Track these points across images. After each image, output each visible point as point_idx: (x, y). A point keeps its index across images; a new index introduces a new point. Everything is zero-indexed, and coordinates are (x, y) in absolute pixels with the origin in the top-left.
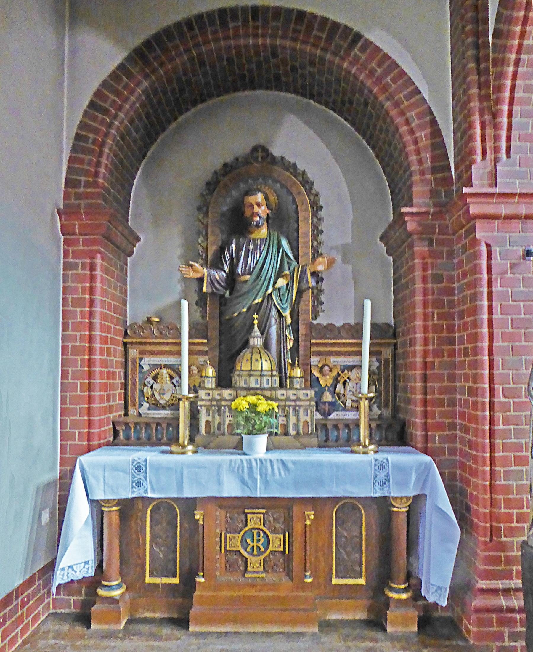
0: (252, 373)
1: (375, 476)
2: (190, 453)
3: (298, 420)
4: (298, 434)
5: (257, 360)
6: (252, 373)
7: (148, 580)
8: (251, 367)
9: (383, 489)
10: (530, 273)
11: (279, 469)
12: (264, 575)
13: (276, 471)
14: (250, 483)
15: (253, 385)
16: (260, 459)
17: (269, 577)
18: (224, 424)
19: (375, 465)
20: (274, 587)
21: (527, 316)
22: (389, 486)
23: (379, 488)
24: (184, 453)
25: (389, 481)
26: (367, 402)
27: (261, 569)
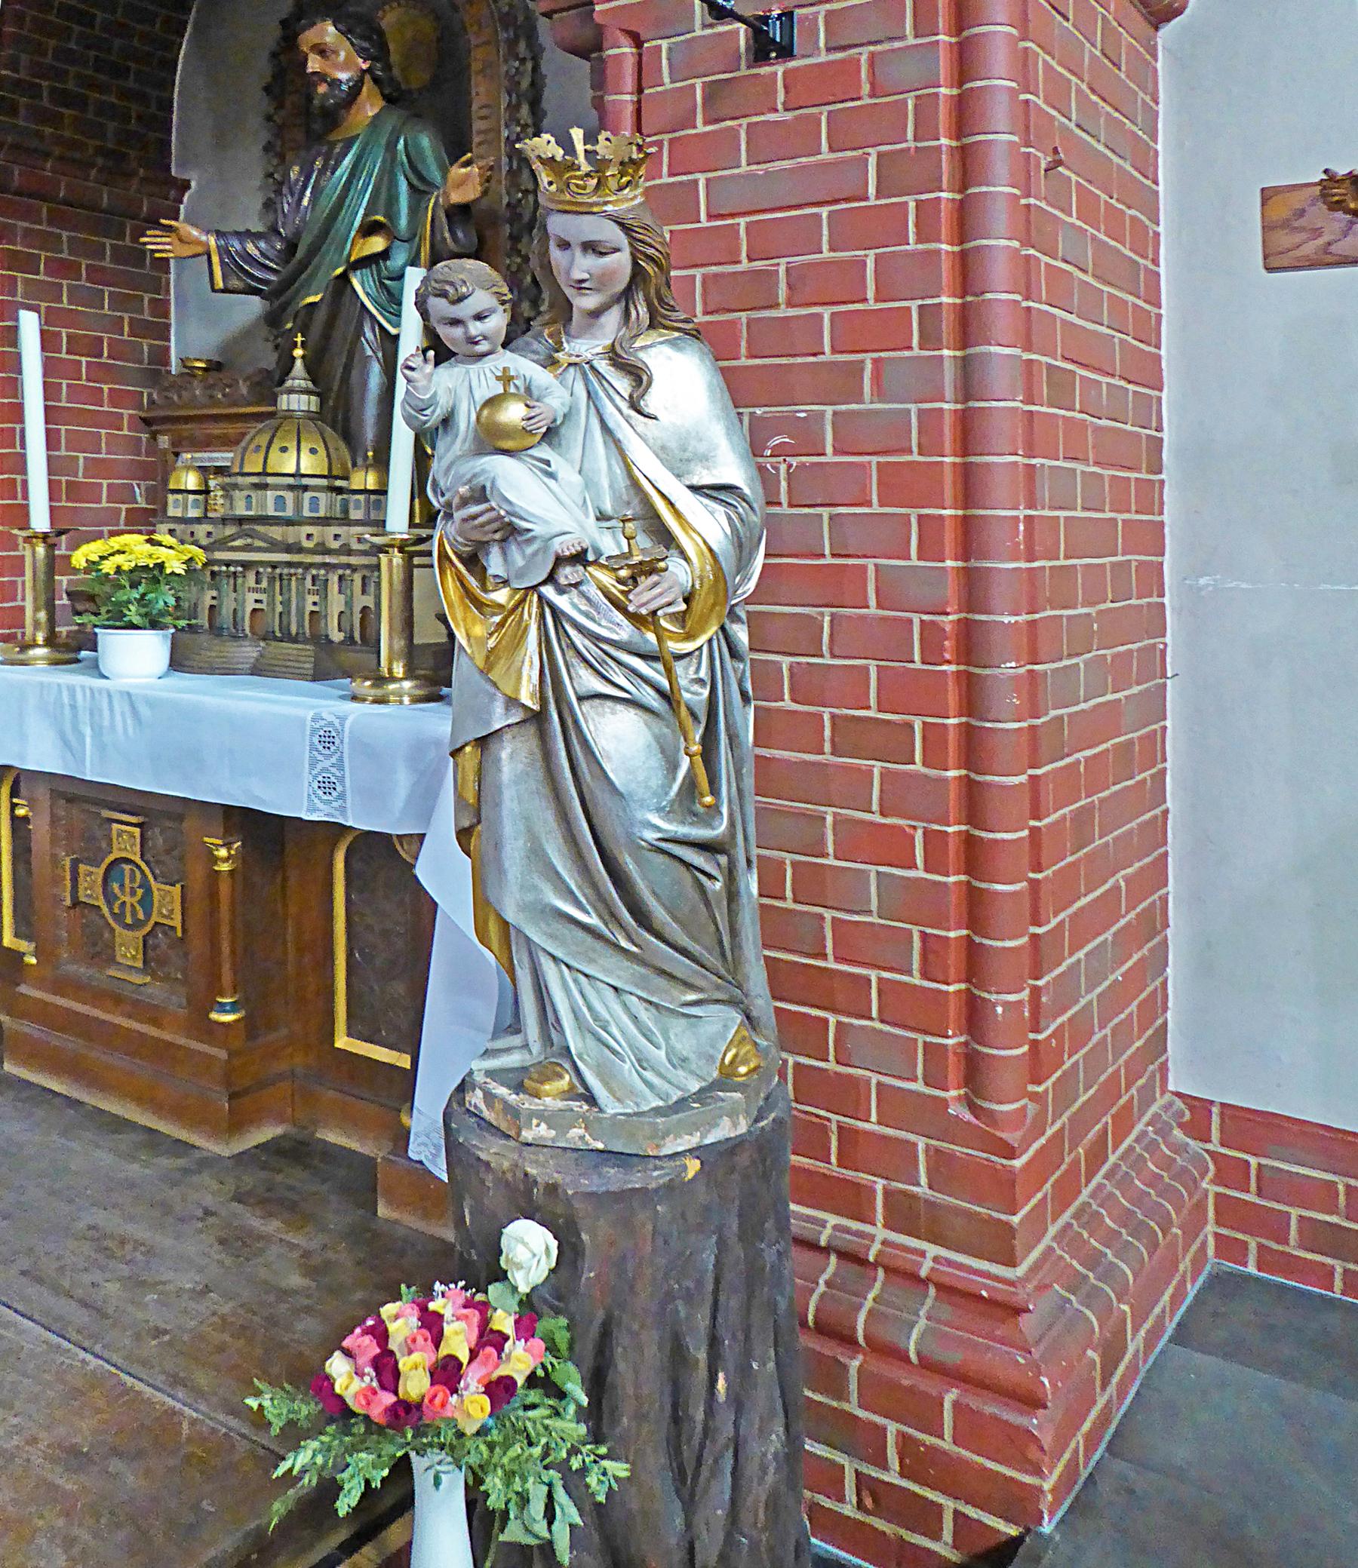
0: (270, 480)
1: (313, 763)
2: (42, 665)
3: (349, 604)
4: (350, 639)
5: (284, 450)
6: (270, 480)
7: (342, 1042)
8: (265, 462)
9: (329, 802)
10: (776, 111)
11: (123, 714)
12: (138, 979)
13: (118, 718)
14: (74, 743)
15: (241, 510)
16: (91, 689)
17: (156, 992)
18: (244, 611)
19: (314, 731)
20: (153, 1015)
21: (758, 264)
22: (342, 796)
23: (320, 799)
24: (23, 663)
25: (342, 780)
26: (397, 558)
27: (140, 964)
